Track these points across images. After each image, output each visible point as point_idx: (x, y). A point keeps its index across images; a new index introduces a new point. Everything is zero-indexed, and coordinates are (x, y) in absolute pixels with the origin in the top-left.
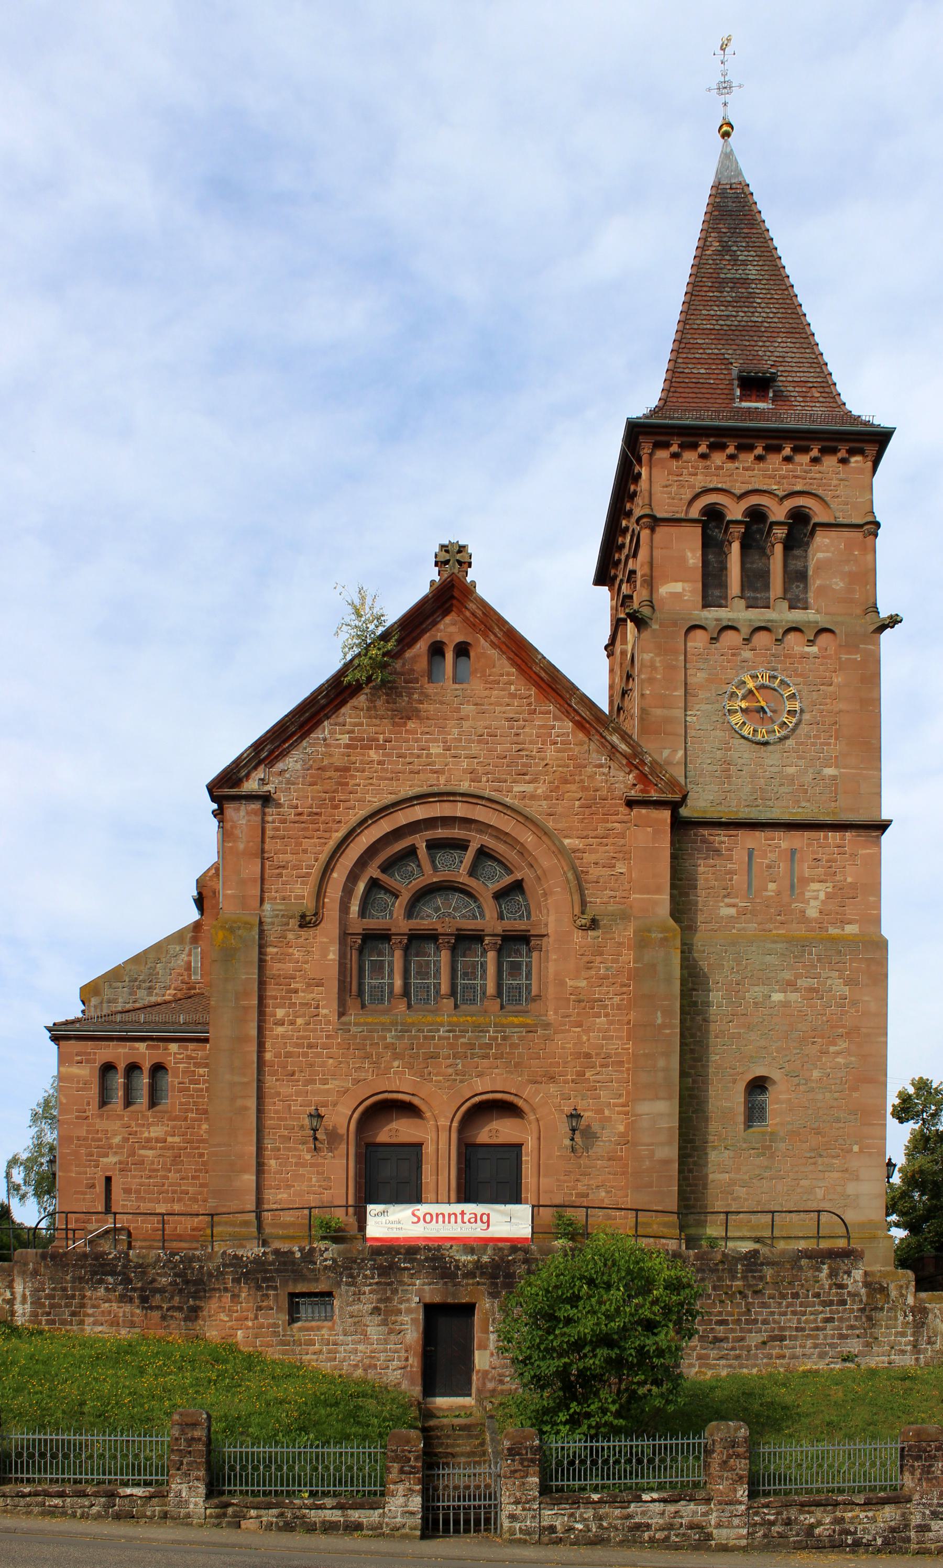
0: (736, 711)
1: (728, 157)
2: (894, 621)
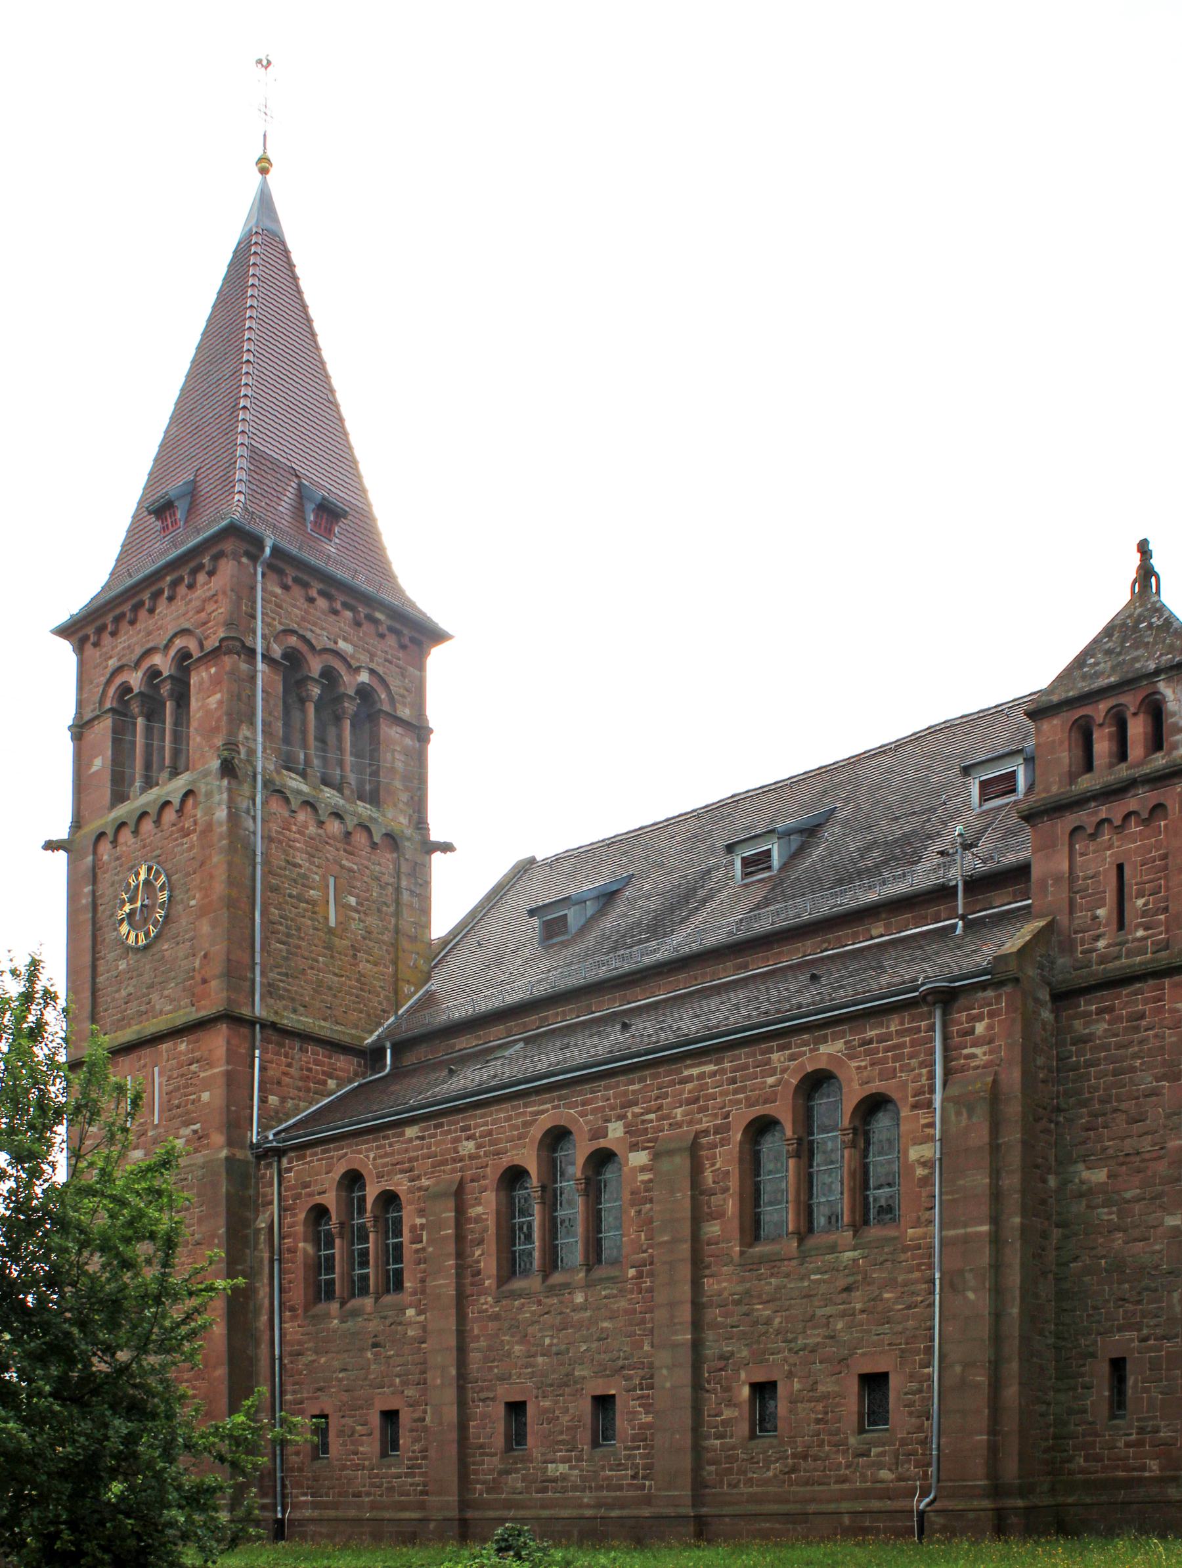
1: (264, 204)
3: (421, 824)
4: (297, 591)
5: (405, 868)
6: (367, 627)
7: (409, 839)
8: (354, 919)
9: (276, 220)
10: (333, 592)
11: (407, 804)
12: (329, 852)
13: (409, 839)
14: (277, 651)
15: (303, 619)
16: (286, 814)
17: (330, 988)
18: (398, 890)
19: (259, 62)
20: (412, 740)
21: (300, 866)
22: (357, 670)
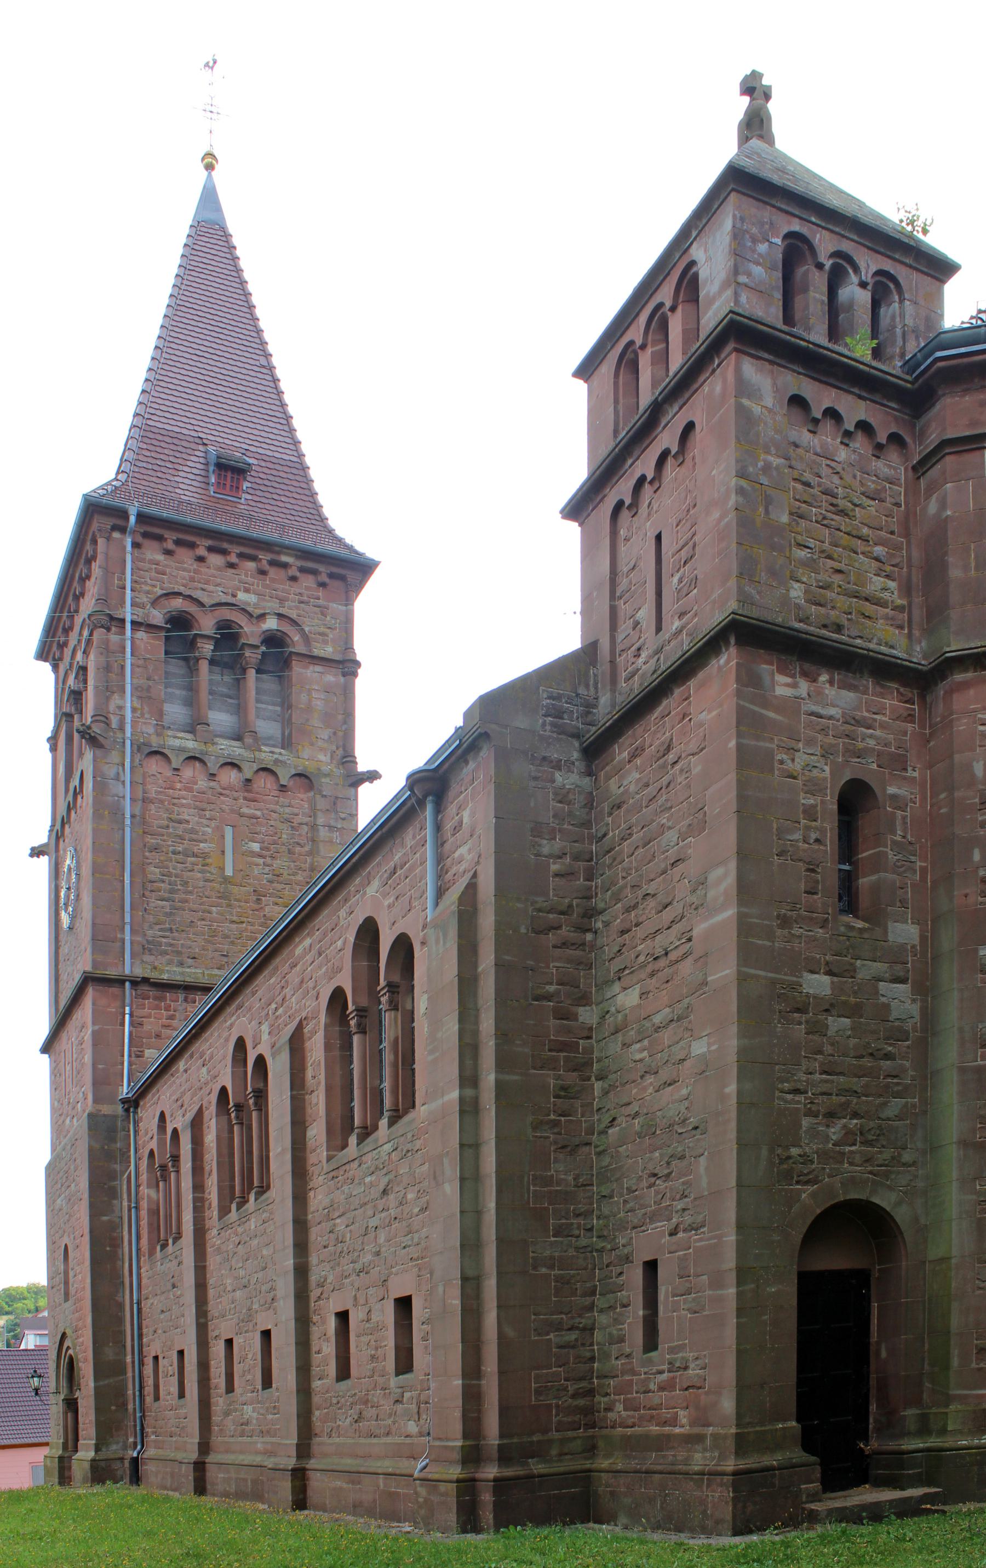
1: (209, 197)
3: (348, 758)
4: (183, 553)
5: (321, 804)
6: (273, 572)
7: (326, 775)
8: (257, 865)
9: (218, 209)
10: (225, 545)
11: (329, 740)
12: (223, 803)
13: (326, 775)
14: (157, 617)
15: (192, 579)
16: (169, 773)
17: (227, 937)
18: (314, 827)
19: (207, 65)
20: (335, 675)
21: (188, 822)
22: (262, 617)
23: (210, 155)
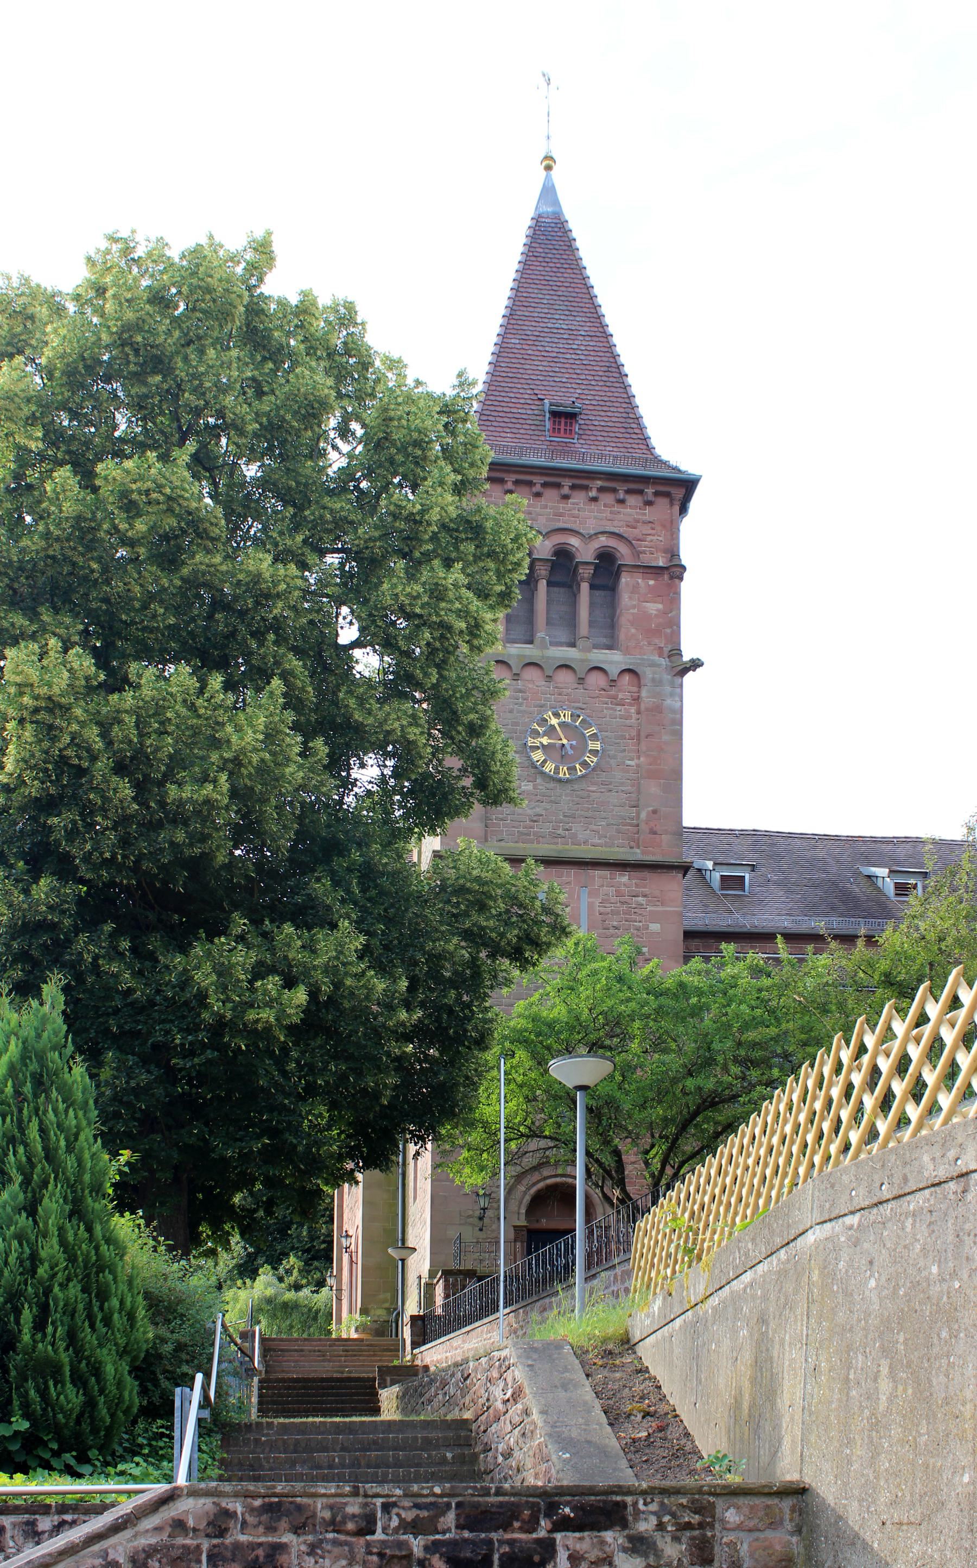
0: (538, 748)
1: (548, 192)
2: (695, 664)
9: (556, 202)
10: (585, 482)
23: (548, 157)
